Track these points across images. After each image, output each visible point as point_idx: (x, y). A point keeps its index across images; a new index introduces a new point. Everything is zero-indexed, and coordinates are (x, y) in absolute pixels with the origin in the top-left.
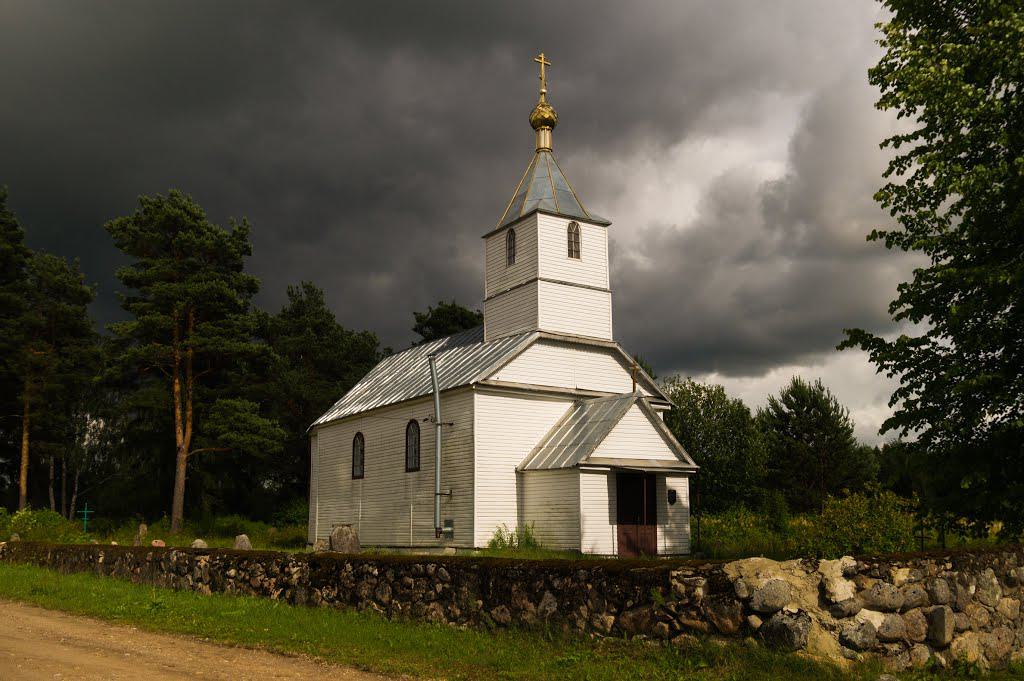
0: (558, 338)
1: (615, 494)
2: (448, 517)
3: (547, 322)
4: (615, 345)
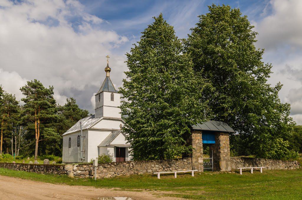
0: (107, 118)
1: (116, 152)
2: (84, 156)
3: (105, 115)
4: (121, 119)
